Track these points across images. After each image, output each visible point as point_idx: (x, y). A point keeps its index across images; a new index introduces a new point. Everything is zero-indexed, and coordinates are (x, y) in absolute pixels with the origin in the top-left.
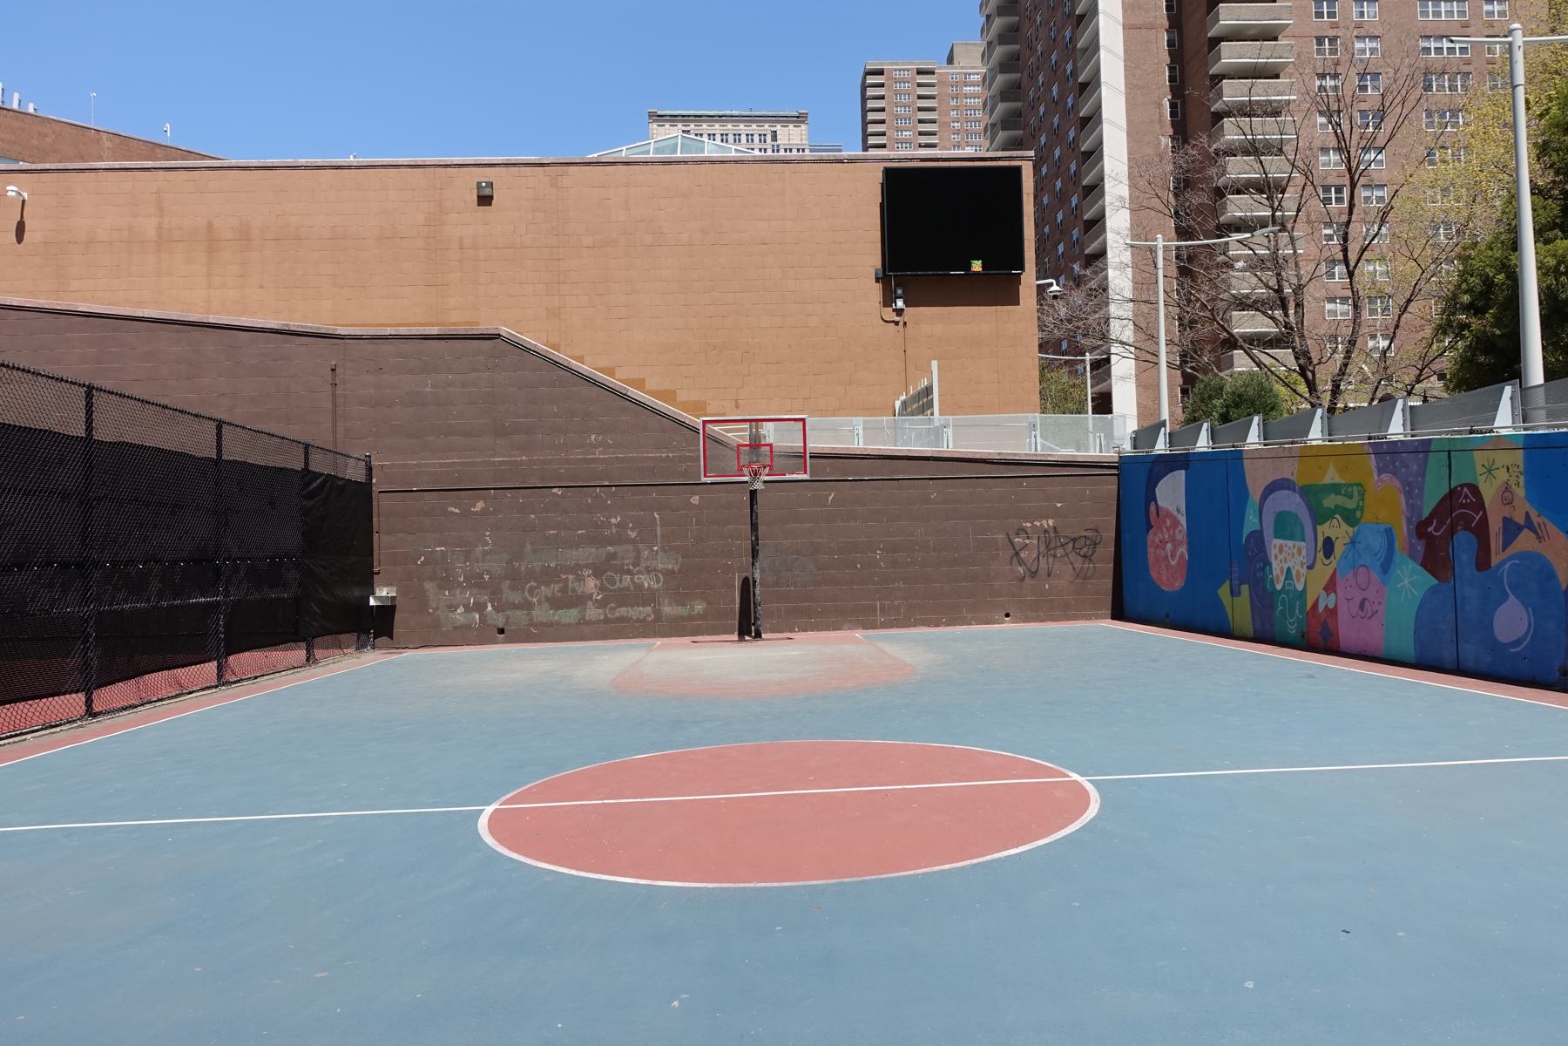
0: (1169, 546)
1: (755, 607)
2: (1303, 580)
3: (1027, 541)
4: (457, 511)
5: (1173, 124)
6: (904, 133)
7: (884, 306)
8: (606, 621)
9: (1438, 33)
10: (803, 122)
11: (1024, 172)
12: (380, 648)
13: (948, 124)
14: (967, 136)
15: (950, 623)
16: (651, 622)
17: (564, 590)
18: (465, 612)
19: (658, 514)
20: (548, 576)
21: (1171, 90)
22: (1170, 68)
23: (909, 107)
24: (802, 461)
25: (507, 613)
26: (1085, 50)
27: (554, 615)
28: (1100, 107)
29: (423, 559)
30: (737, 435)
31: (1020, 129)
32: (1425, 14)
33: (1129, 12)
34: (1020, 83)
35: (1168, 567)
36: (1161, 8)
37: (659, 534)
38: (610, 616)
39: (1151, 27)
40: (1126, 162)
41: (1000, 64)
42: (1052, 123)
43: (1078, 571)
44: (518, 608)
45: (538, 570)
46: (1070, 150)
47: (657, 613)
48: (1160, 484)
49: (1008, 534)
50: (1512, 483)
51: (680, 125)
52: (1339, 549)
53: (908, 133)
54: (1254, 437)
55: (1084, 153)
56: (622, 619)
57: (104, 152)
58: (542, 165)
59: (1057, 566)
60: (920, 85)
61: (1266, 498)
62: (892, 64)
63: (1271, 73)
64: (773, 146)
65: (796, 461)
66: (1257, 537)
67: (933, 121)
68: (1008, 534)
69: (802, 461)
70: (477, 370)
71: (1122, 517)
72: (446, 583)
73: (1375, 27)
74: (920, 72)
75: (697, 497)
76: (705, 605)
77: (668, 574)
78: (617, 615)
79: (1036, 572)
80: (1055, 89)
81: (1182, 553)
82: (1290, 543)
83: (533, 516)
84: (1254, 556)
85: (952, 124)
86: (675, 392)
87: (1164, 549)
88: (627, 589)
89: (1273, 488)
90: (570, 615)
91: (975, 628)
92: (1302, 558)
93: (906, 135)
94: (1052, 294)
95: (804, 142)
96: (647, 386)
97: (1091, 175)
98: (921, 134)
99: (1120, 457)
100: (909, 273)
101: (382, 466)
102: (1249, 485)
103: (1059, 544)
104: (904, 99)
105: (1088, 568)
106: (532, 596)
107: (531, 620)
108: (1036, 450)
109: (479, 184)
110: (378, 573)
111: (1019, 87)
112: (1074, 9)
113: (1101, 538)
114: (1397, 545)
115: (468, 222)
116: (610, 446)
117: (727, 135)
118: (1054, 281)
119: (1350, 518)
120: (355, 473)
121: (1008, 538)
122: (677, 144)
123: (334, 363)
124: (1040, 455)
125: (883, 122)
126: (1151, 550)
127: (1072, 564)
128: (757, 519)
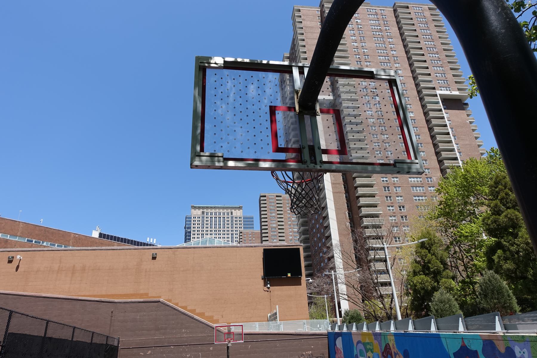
4: (143, 354)
5: (350, 219)
6: (273, 214)
13: (286, 211)
19: (201, 353)
21: (348, 210)
22: (347, 204)
23: (274, 206)
24: (242, 336)
26: (323, 198)
39: (340, 193)
40: (337, 230)
42: (315, 217)
48: (337, 340)
49: (299, 356)
51: (201, 210)
53: (274, 214)
54: (354, 329)
55: (325, 227)
57: (20, 228)
58: (171, 248)
60: (277, 200)
61: (358, 344)
62: (268, 194)
63: (375, 206)
66: (357, 355)
68: (299, 356)
69: (242, 336)
70: (152, 311)
74: (277, 196)
75: (212, 348)
83: (164, 355)
86: (204, 313)
89: (359, 342)
95: (241, 215)
96: (196, 311)
98: (278, 214)
101: (122, 341)
104: (273, 204)
109: (153, 254)
115: (149, 264)
116: (188, 333)
118: (310, 279)
123: (112, 310)
124: (306, 332)
128: (229, 354)
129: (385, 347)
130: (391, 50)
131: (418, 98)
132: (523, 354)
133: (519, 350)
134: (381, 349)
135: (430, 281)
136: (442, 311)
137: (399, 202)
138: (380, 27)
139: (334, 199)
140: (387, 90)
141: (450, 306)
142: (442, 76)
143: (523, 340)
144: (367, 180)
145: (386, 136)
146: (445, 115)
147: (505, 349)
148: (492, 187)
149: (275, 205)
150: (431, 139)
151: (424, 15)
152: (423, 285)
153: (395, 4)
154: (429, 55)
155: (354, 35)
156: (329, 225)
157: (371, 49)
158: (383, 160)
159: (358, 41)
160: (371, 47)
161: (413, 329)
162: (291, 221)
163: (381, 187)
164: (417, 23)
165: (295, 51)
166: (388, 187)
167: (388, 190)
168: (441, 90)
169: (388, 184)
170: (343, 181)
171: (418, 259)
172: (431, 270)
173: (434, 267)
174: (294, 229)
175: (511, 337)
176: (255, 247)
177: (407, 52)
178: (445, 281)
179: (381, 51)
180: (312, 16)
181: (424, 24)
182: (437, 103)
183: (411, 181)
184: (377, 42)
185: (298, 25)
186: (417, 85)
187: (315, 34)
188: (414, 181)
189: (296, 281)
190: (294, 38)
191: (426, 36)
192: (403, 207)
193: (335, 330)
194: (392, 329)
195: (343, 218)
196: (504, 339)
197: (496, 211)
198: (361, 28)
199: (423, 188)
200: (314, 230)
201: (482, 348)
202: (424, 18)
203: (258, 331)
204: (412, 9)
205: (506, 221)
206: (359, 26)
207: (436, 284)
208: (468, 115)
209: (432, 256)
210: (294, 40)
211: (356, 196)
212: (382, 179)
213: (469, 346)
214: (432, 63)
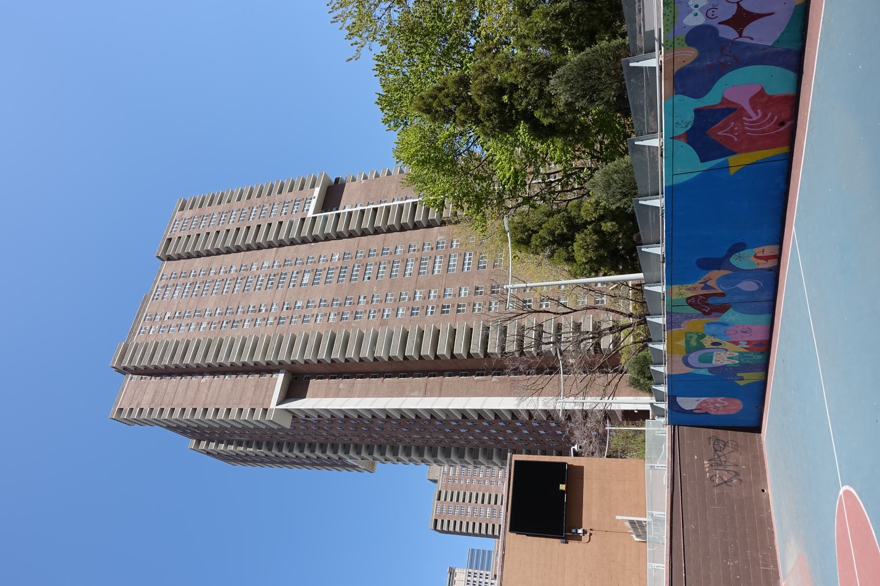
0: (717, 405)
3: (718, 476)
6: (469, 511)
7: (581, 541)
10: (454, 570)
14: (474, 475)
15: (771, 525)
21: (471, 376)
22: (461, 376)
23: (456, 506)
26: (447, 416)
28: (475, 410)
31: (479, 449)
33: (433, 394)
34: (457, 448)
36: (433, 379)
40: (502, 398)
41: (446, 457)
42: (478, 433)
43: (734, 450)
49: (714, 486)
50: (686, 288)
52: (717, 340)
53: (469, 509)
54: (661, 369)
55: (495, 418)
59: (731, 461)
60: (445, 500)
61: (688, 364)
62: (433, 514)
66: (711, 370)
67: (465, 494)
68: (714, 486)
71: (701, 425)
73: (456, 289)
74: (439, 499)
79: (735, 472)
80: (463, 431)
81: (720, 400)
82: (714, 357)
84: (720, 371)
87: (719, 407)
89: (686, 363)
91: (773, 510)
94: (579, 449)
95: (465, 572)
99: (669, 424)
100: (564, 524)
102: (686, 372)
103: (718, 459)
105: (731, 444)
108: (665, 467)
111: (458, 448)
112: (428, 420)
113: (714, 436)
114: (714, 321)
118: (573, 447)
121: (716, 486)
124: (668, 465)
126: (719, 413)
127: (730, 453)
129: (694, 308)
130: (228, 272)
131: (312, 244)
132: (699, 8)
133: (691, 16)
134: (697, 317)
135: (583, 236)
136: (624, 186)
137: (469, 294)
138: (188, 284)
139: (450, 397)
140: (290, 288)
141: (616, 172)
142: (287, 206)
143: (672, 5)
144: (426, 337)
145: (361, 300)
146: (347, 210)
147: (690, 48)
148: (435, 116)
149: (454, 504)
150: (379, 234)
151: (189, 219)
152: (590, 247)
153: (158, 257)
154: (251, 220)
155: (189, 325)
156: (492, 410)
157: (219, 303)
158: (398, 308)
159: (200, 320)
160: (216, 302)
161: (659, 247)
162: (484, 478)
163: (442, 318)
164: (198, 229)
165: (189, 428)
166: (444, 307)
167: (448, 307)
168: (308, 210)
169: (438, 306)
170: (424, 376)
171: (548, 252)
172: (565, 231)
173: (560, 226)
174: (500, 475)
175: (668, 30)
176: (504, 549)
177: (238, 250)
178: (585, 212)
179: (226, 288)
180: (137, 390)
181: (202, 221)
182: (326, 218)
183: (439, 271)
184: (210, 292)
185: (135, 415)
186: (293, 243)
187: (168, 389)
188: (439, 267)
189: (574, 476)
190: (165, 425)
191: (220, 220)
192: (477, 289)
193: (664, 409)
194: (660, 289)
195: (484, 385)
196: (671, 46)
197: (472, 113)
198: (180, 313)
199: (453, 255)
200: (501, 438)
201: (691, 97)
202: (192, 220)
203: (664, 565)
204: (174, 235)
205: (488, 98)
206: (177, 315)
207: (590, 227)
208: (354, 180)
209: (542, 229)
210: (169, 427)
211: (451, 358)
212: (429, 314)
213: (686, 126)
214: (263, 217)
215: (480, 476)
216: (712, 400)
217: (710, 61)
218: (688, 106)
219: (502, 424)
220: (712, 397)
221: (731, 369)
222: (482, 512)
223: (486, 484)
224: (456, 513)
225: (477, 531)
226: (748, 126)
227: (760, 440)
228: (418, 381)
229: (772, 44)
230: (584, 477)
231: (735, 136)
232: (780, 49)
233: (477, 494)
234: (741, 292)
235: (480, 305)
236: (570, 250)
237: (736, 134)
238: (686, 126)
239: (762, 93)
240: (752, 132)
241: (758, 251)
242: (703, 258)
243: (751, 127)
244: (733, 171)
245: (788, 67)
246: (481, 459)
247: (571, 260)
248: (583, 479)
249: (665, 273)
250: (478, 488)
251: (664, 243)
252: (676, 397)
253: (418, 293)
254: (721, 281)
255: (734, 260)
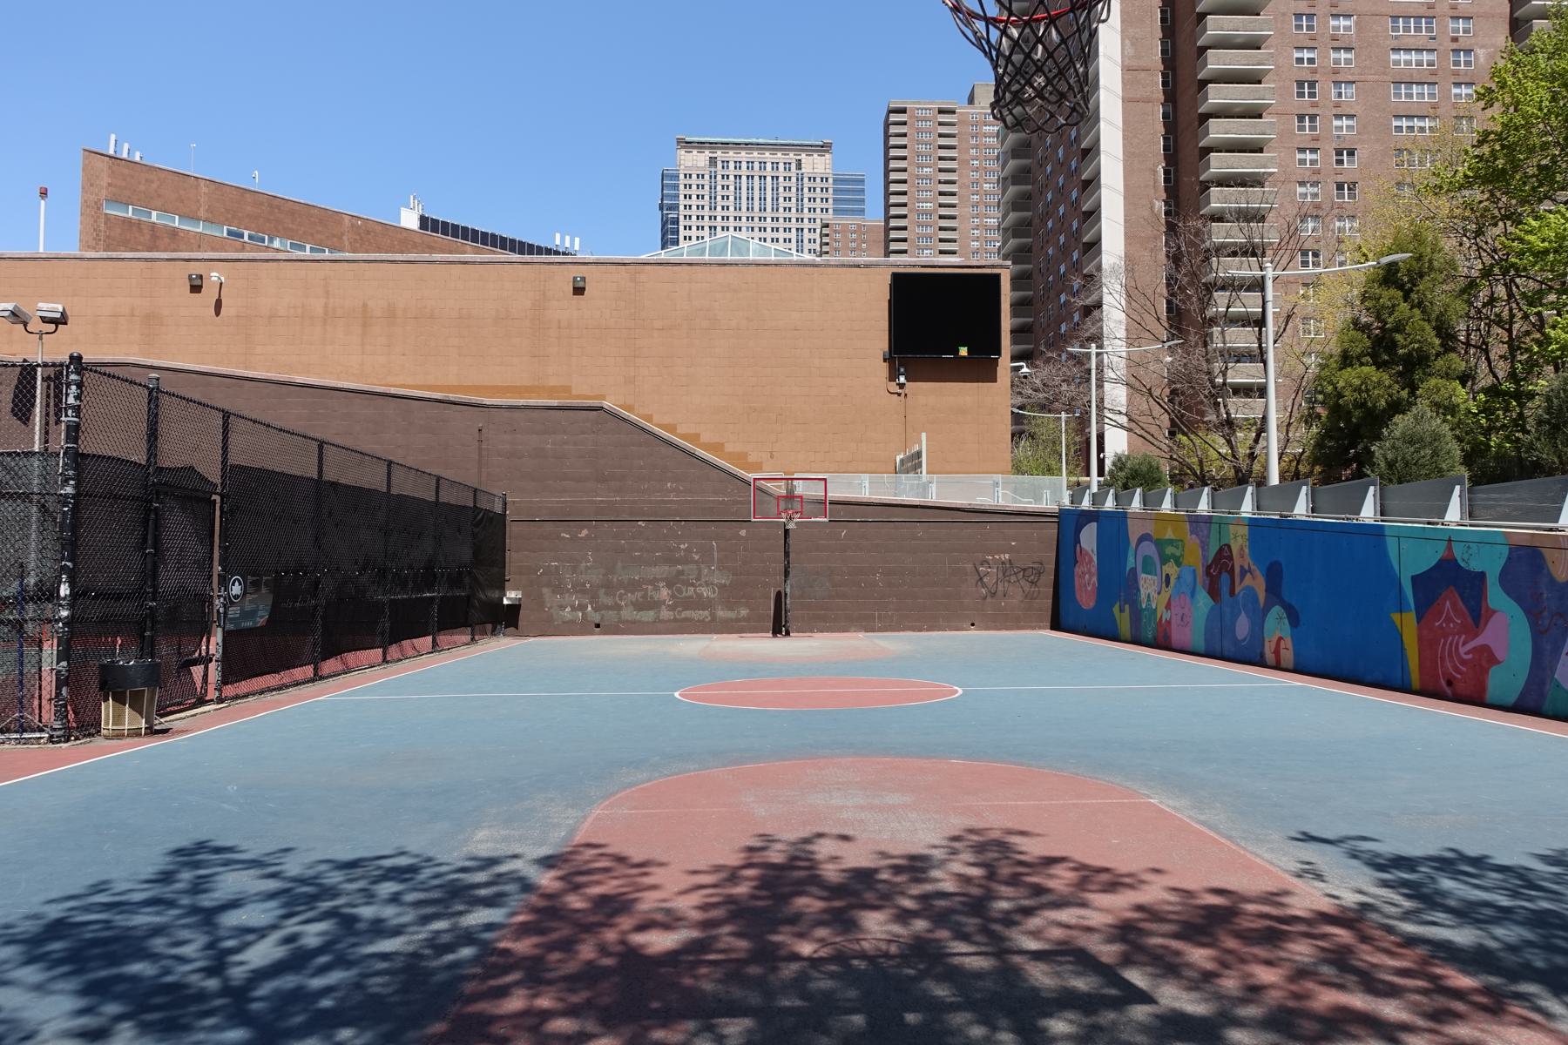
0: (1087, 576)
1: (786, 613)
2: (1155, 601)
3: (989, 570)
4: (568, 536)
6: (925, 170)
8: (675, 620)
9: (1409, 114)
10: (827, 151)
11: (1002, 278)
12: (508, 636)
16: (709, 621)
17: (644, 597)
18: (572, 610)
20: (633, 586)
21: (1165, 159)
22: (1164, 138)
23: (930, 145)
24: (823, 506)
25: (602, 612)
27: (636, 615)
28: (1099, 173)
29: (541, 571)
30: (780, 489)
32: (1398, 95)
35: (1086, 590)
37: (716, 557)
38: (678, 617)
39: (1147, 101)
40: (1122, 223)
42: (1058, 183)
44: (611, 610)
45: (626, 582)
46: (1073, 209)
47: (713, 616)
51: (707, 152)
53: (928, 170)
54: (1136, 504)
55: (1084, 213)
56: (686, 619)
62: (914, 103)
64: (798, 174)
65: (818, 506)
66: (1134, 570)
67: (953, 159)
69: (823, 506)
70: (583, 433)
72: (558, 588)
74: (941, 111)
76: (748, 611)
77: (722, 587)
78: (683, 616)
79: (994, 594)
80: (1061, 151)
82: (1150, 577)
83: (623, 542)
85: (972, 162)
86: (723, 444)
88: (691, 597)
89: (1142, 539)
90: (648, 616)
92: (1155, 588)
93: (926, 172)
95: (828, 171)
97: (1091, 233)
98: (941, 170)
101: (514, 502)
104: (926, 137)
105: (1034, 592)
106: (621, 600)
107: (620, 618)
110: (509, 580)
115: (565, 308)
117: (752, 162)
119: (1178, 564)
120: (498, 509)
122: (728, 242)
125: (904, 158)
126: (1076, 579)
127: (1022, 587)
134: (1205, 557)
136: (1407, 464)
137: (1339, 137)
141: (1435, 453)
161: (1307, 510)
166: (1312, 84)
170: (1164, 61)
174: (988, 220)
176: (867, 266)
188: (1408, 63)
194: (1247, 508)
200: (1050, 224)
203: (867, 495)
207: (1404, 394)
212: (1297, 55)
213: (1464, 560)
215: (985, 185)
216: (1094, 570)
217: (1548, 598)
218: (1491, 564)
219: (1075, 224)
220: (1098, 569)
221: (1134, 598)
222: (925, 193)
223: (972, 197)
224: (920, 146)
225: (893, 187)
226: (1453, 640)
227: (1040, 628)
228: (1154, 51)
229: (1556, 680)
230: (980, 384)
231: (1442, 623)
232: (1548, 687)
233: (953, 182)
234: (1235, 617)
235: (1313, 162)
236: (1364, 360)
237: (1444, 625)
238: (1464, 560)
239: (1493, 660)
240: (1444, 644)
241: (1288, 642)
242: (1282, 571)
243: (1451, 644)
244: (1396, 617)
245: (1523, 695)
246: (1012, 190)
247: (1345, 361)
248: (978, 382)
249: (1266, 516)
250: (964, 184)
251: (1311, 519)
252: (1097, 522)
253: (1347, 23)
254: (1251, 591)
255: (1277, 610)
